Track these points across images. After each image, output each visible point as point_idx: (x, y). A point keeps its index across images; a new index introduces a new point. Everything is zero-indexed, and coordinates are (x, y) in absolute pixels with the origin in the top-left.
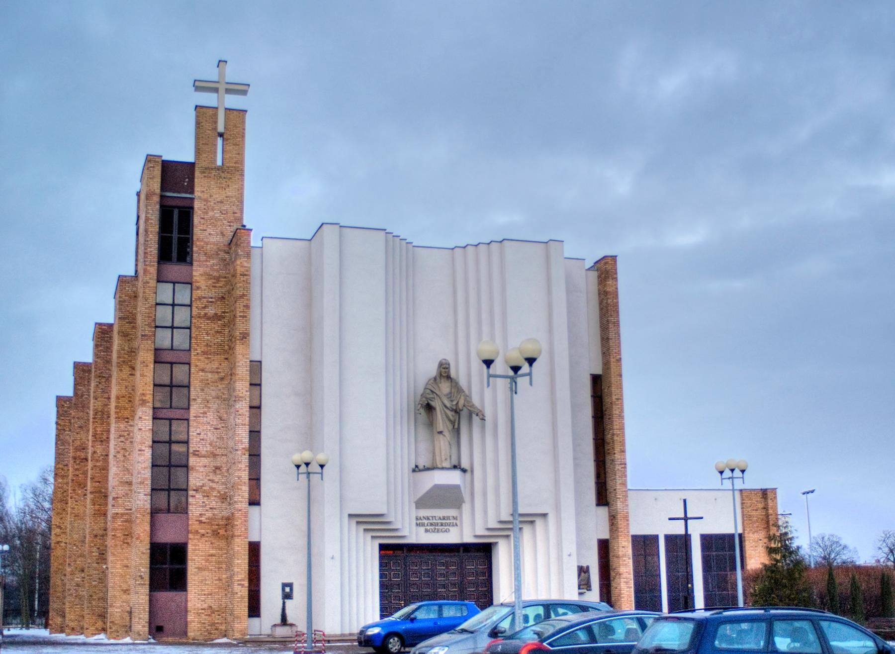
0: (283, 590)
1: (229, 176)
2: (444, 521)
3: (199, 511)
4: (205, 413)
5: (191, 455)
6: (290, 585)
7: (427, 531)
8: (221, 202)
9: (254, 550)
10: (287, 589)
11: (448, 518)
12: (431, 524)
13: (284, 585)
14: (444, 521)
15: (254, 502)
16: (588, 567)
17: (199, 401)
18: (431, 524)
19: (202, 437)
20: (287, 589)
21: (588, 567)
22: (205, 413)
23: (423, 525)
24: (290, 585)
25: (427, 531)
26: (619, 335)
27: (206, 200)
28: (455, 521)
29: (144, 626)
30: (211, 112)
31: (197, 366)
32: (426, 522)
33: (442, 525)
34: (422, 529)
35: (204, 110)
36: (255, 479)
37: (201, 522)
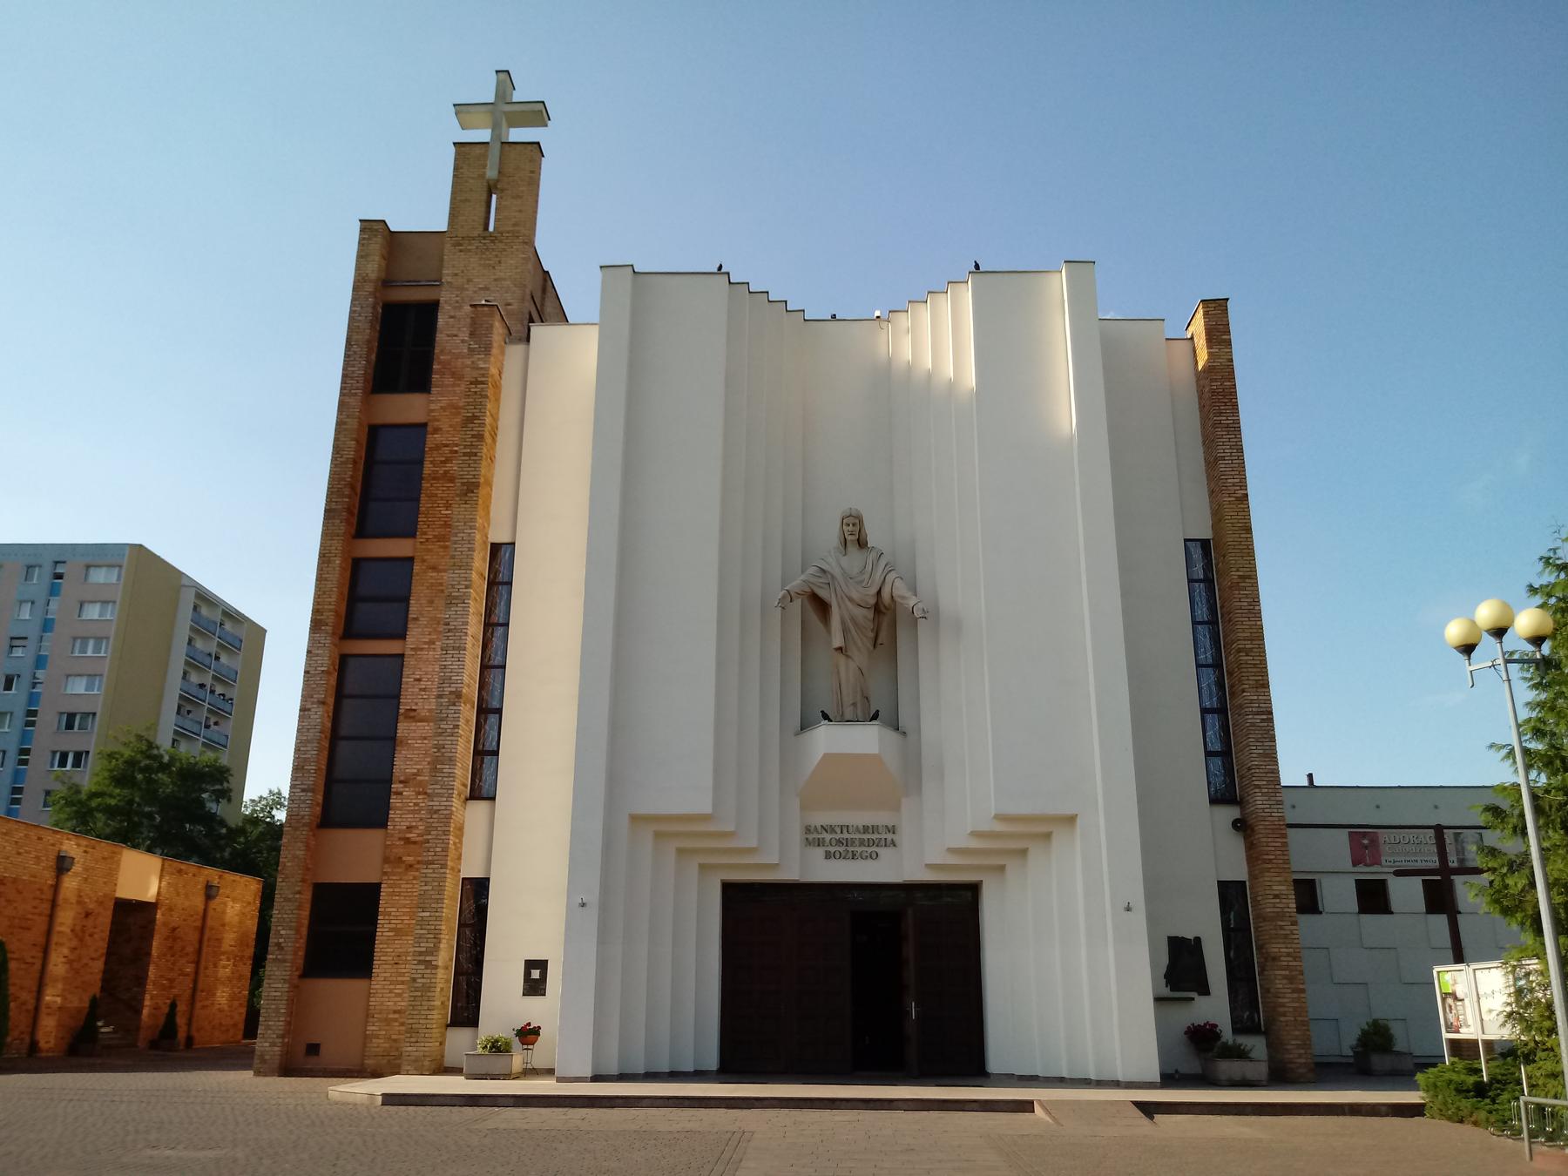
0: (527, 974)
1: (501, 246)
2: (866, 837)
3: (409, 819)
4: (432, 642)
5: (401, 718)
6: (542, 965)
7: (828, 856)
8: (486, 289)
9: (477, 890)
10: (536, 974)
11: (875, 829)
12: (839, 842)
13: (530, 965)
14: (866, 837)
15: (481, 791)
16: (1198, 940)
17: (423, 621)
18: (839, 842)
19: (423, 685)
20: (536, 974)
21: (1198, 940)
22: (432, 642)
23: (820, 843)
24: (542, 965)
25: (828, 856)
26: (1241, 450)
27: (462, 289)
28: (889, 836)
29: (273, 1044)
30: (478, 150)
31: (424, 561)
32: (828, 837)
33: (862, 843)
34: (819, 852)
35: (467, 148)
36: (486, 753)
37: (408, 841)
